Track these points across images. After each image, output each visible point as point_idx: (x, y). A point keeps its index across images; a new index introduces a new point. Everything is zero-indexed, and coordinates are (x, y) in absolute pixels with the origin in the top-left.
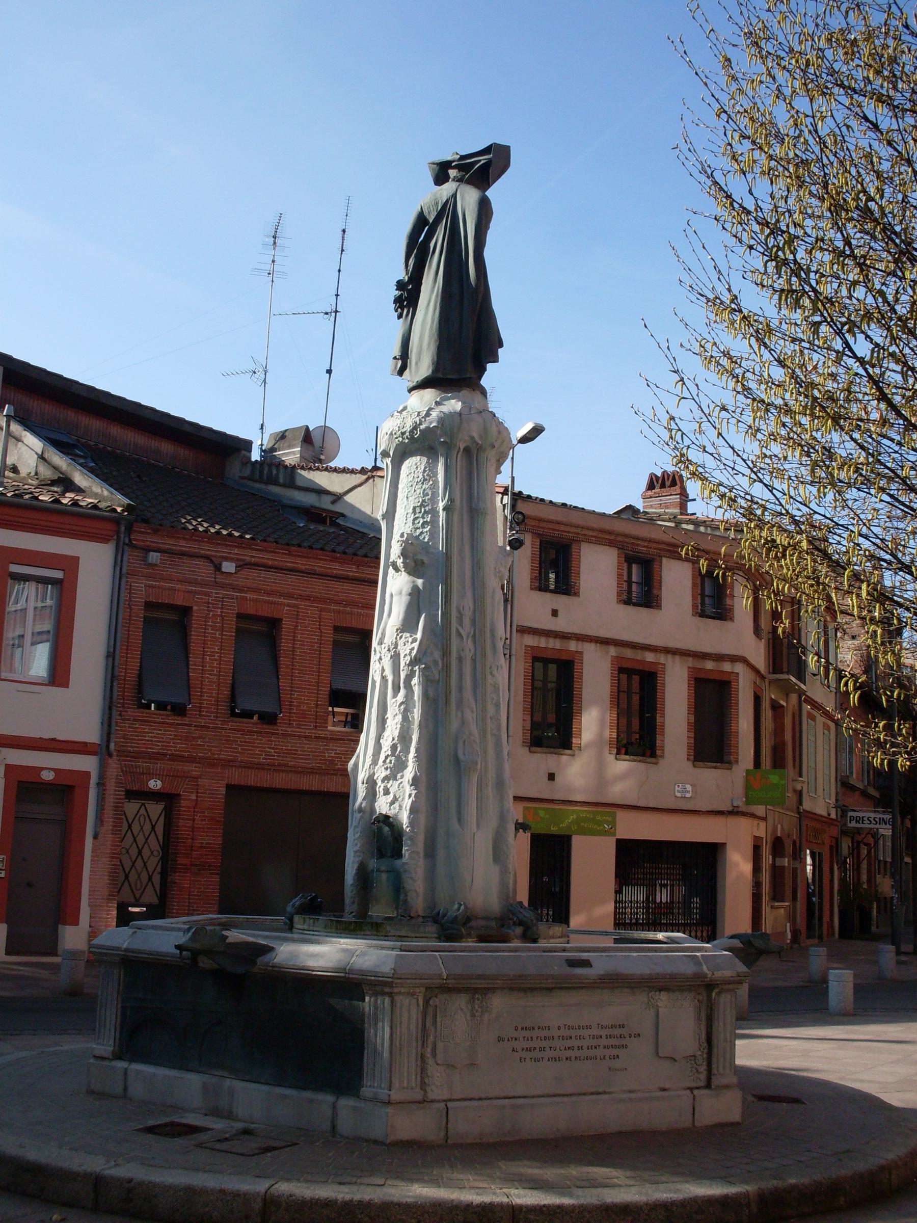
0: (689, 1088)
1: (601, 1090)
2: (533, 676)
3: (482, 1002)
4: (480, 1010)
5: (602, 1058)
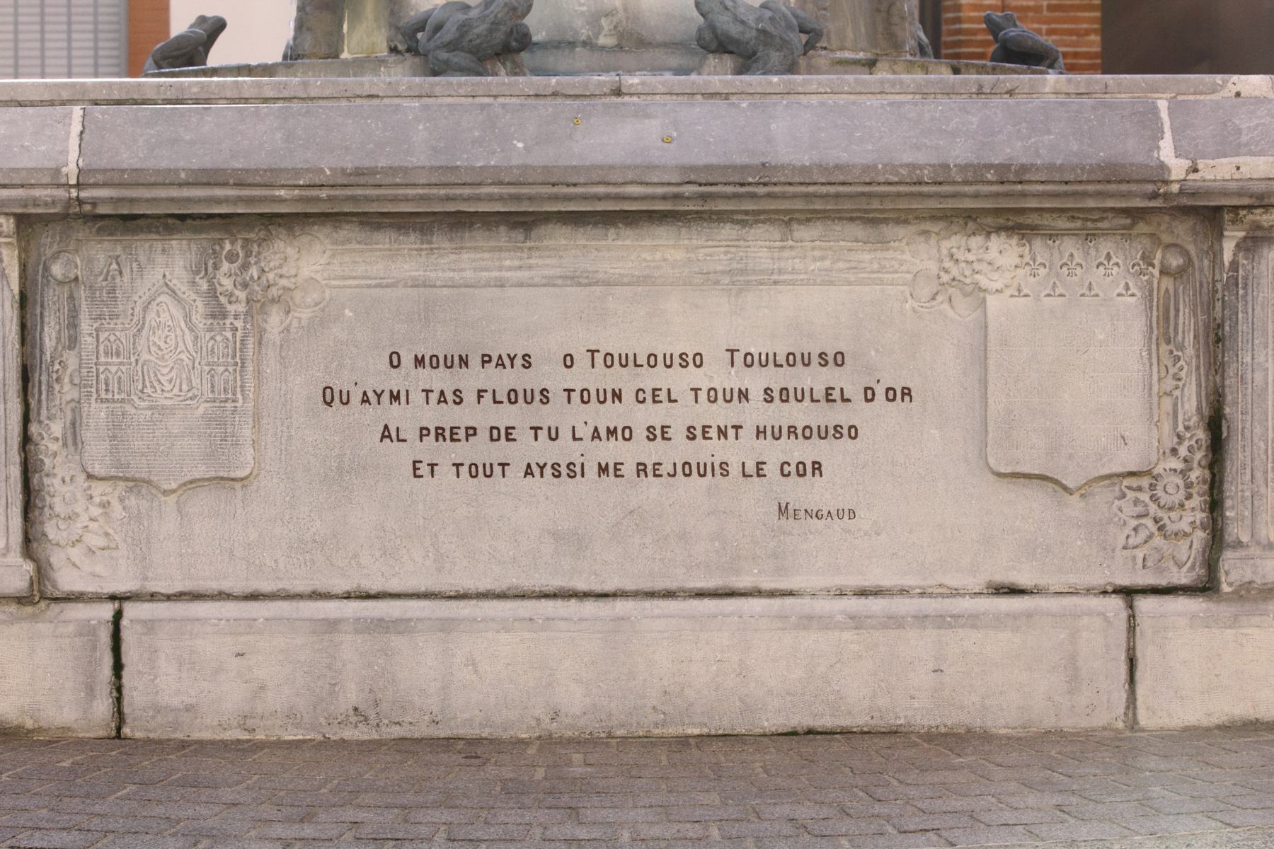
1: (743, 582)
3: (245, 267)
4: (242, 295)
5: (751, 468)
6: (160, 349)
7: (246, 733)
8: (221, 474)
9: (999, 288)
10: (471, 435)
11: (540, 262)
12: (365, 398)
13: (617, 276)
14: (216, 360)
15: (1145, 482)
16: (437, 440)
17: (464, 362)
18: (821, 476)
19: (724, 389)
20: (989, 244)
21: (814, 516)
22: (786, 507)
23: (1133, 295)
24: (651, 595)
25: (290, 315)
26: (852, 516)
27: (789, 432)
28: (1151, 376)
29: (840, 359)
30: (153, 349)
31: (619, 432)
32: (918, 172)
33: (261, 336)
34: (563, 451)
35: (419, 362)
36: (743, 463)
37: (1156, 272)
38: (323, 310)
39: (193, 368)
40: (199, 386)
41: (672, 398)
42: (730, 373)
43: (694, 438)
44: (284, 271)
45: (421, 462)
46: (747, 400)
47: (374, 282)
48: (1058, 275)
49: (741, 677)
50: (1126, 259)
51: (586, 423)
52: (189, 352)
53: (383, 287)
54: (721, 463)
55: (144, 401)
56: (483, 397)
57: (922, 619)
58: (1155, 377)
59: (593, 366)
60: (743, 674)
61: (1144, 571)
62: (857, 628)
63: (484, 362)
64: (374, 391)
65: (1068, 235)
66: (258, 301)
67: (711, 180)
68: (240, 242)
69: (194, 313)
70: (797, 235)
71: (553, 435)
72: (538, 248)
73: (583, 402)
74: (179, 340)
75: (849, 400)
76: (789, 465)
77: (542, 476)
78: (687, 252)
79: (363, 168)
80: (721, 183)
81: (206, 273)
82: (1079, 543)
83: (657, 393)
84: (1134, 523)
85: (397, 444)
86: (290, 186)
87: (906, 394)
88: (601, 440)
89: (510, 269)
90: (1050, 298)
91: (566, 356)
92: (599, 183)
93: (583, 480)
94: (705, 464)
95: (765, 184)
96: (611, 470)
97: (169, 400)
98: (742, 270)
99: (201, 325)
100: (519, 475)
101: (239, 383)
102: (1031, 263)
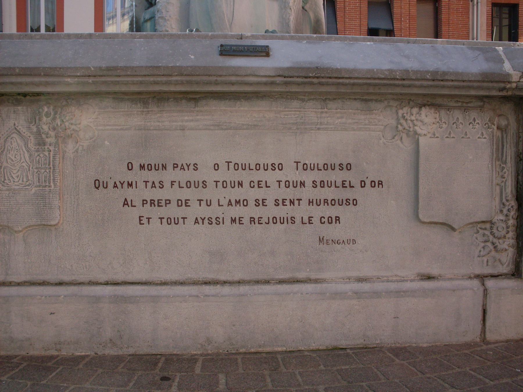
0: (477, 276)
1: (301, 275)
2: (492, 15)
3: (54, 119)
4: (52, 133)
5: (306, 220)
6: (12, 161)
7: (56, 352)
8: (43, 223)
9: (425, 134)
10: (168, 204)
11: (202, 117)
12: (115, 185)
13: (241, 125)
14: (40, 166)
15: (488, 226)
16: (151, 206)
17: (164, 167)
18: (340, 223)
19: (293, 181)
20: (421, 112)
21: (336, 243)
22: (323, 238)
23: (485, 138)
24: (258, 282)
25: (78, 145)
26: (354, 243)
27: (324, 202)
28: (493, 176)
29: (349, 166)
30: (9, 161)
31: (241, 202)
32: (394, 73)
33: (64, 154)
34: (214, 211)
35: (142, 167)
36: (302, 217)
37: (495, 127)
38: (94, 141)
39: (29, 170)
40: (32, 179)
41: (268, 185)
42: (296, 173)
43: (278, 205)
44: (73, 121)
45: (143, 217)
46: (304, 187)
47: (119, 128)
48: (451, 127)
49: (302, 323)
50: (482, 121)
51: (225, 197)
52: (27, 162)
53: (124, 130)
54: (292, 217)
55: (5, 186)
56: (174, 184)
57: (389, 293)
58: (494, 177)
59: (228, 170)
60: (303, 322)
61: (488, 267)
62: (358, 298)
63: (174, 167)
64: (120, 182)
65: (456, 109)
66: (61, 137)
67: (291, 75)
68: (52, 107)
69: (30, 143)
70: (329, 106)
71: (209, 204)
72: (201, 111)
73: (223, 187)
74: (22, 156)
75: (353, 187)
76: (324, 218)
77: (203, 224)
78: (275, 114)
79: (110, 67)
80: (296, 76)
81: (35, 123)
82: (458, 254)
83: (260, 183)
84: (483, 245)
85: (131, 208)
86: (73, 76)
87: (380, 184)
88: (232, 206)
89: (187, 121)
90: (448, 139)
91: (215, 165)
92: (232, 75)
93: (224, 225)
94: (284, 218)
95: (318, 78)
96: (237, 221)
97: (17, 186)
98: (302, 123)
99: (33, 149)
100: (191, 223)
101: (52, 178)
102: (440, 122)
